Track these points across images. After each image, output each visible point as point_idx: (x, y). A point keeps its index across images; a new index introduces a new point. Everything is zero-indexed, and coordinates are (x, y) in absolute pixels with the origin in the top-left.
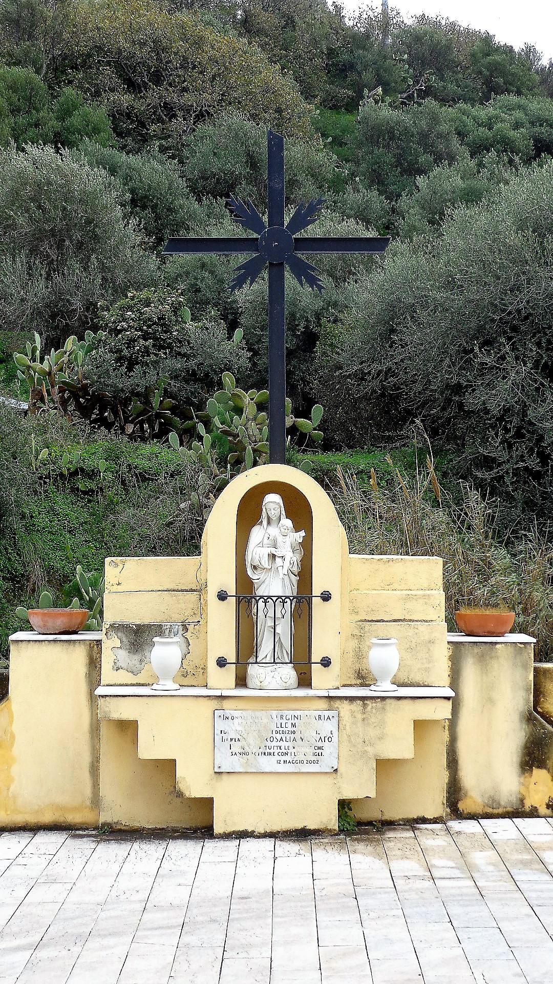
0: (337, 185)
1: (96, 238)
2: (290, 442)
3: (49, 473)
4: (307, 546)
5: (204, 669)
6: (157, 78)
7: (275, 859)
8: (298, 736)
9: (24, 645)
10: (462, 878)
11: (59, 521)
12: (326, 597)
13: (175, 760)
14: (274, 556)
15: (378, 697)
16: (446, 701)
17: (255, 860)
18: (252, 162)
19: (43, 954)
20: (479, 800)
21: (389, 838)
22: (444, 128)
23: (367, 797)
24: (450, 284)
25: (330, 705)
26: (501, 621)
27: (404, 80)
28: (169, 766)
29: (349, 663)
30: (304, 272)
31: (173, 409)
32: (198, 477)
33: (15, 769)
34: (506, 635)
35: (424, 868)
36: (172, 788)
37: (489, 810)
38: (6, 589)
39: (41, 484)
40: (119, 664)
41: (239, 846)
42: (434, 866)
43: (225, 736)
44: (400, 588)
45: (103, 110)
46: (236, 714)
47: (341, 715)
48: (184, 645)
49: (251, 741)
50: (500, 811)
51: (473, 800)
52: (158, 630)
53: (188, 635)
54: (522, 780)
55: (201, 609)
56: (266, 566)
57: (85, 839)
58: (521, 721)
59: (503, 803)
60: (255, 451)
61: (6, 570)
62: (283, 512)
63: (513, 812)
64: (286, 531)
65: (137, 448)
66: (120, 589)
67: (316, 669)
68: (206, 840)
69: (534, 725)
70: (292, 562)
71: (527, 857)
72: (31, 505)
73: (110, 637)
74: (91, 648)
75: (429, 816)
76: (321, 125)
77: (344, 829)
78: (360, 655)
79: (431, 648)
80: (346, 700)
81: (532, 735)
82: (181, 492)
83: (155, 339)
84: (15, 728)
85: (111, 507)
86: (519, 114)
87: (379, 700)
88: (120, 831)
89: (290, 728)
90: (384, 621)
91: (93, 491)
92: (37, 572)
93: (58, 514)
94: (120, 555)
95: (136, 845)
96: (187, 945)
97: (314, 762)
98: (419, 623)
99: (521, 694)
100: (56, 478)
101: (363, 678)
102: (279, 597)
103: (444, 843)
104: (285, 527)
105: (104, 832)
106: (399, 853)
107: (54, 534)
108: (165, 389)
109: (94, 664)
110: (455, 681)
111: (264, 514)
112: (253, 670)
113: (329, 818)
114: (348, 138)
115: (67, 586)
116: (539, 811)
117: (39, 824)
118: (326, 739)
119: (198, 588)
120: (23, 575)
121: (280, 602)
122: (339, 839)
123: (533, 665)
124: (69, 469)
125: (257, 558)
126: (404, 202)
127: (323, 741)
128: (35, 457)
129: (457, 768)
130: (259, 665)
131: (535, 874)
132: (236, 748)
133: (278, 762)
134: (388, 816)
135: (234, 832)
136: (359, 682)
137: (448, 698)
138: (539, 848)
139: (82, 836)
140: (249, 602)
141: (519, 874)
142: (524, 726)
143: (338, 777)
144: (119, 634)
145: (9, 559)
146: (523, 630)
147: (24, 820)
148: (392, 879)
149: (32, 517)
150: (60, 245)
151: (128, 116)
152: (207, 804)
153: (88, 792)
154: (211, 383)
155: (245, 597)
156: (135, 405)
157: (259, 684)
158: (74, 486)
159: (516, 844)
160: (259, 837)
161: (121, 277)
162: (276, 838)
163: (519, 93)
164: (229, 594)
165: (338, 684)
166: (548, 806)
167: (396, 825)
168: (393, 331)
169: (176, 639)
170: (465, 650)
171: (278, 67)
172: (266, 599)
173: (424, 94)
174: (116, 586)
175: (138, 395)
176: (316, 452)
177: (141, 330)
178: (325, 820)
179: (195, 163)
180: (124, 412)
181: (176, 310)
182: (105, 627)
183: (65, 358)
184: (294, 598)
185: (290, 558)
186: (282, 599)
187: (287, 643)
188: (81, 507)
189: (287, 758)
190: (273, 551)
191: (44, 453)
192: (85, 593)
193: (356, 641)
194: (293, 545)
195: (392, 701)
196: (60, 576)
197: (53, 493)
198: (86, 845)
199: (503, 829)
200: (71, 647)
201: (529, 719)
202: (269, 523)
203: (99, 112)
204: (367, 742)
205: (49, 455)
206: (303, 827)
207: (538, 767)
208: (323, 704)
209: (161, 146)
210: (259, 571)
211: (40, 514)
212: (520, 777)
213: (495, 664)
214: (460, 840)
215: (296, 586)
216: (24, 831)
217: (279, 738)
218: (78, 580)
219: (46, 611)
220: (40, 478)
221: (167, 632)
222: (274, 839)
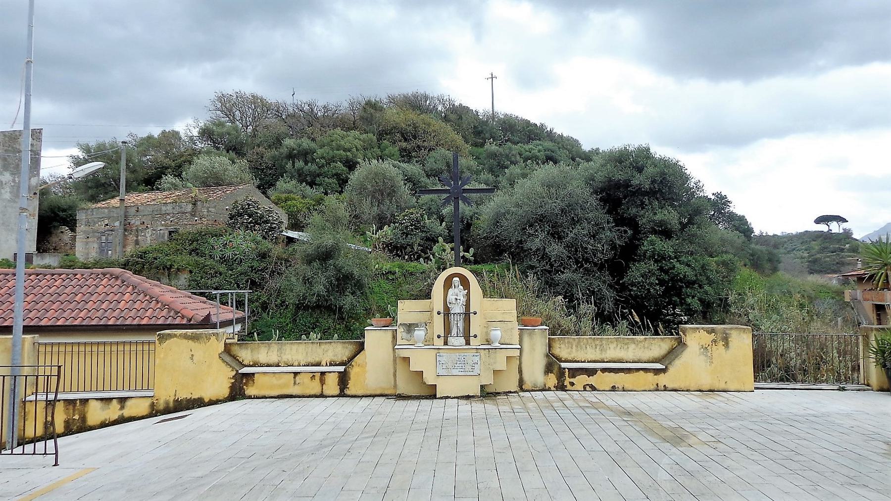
0: (478, 173)
1: (394, 191)
4: (468, 295)
5: (433, 339)
6: (415, 137)
8: (466, 363)
14: (457, 299)
18: (448, 165)
19: (376, 439)
22: (513, 152)
24: (518, 205)
27: (500, 136)
30: (466, 201)
31: (422, 250)
37: (533, 388)
45: (397, 148)
48: (426, 331)
51: (528, 385)
52: (417, 325)
54: (545, 377)
55: (432, 317)
56: (454, 303)
57: (392, 399)
60: (450, 264)
62: (460, 284)
72: (372, 284)
76: (472, 152)
78: (487, 333)
83: (415, 226)
86: (540, 147)
96: (427, 436)
99: (544, 347)
101: (488, 342)
106: (502, 404)
108: (419, 243)
109: (394, 338)
110: (521, 343)
114: (480, 157)
126: (500, 179)
134: (498, 391)
137: (518, 349)
139: (390, 398)
142: (545, 358)
145: (365, 303)
150: (382, 194)
151: (405, 150)
154: (435, 241)
156: (409, 249)
161: (403, 205)
163: (540, 140)
166: (554, 387)
168: (498, 222)
171: (456, 132)
172: (454, 314)
173: (506, 141)
175: (409, 245)
177: (410, 223)
179: (428, 166)
180: (405, 252)
181: (422, 216)
183: (384, 233)
185: (463, 300)
198: (392, 401)
199: (539, 395)
201: (547, 356)
203: (395, 150)
208: (475, 351)
209: (416, 161)
219: (378, 319)
220: (376, 275)
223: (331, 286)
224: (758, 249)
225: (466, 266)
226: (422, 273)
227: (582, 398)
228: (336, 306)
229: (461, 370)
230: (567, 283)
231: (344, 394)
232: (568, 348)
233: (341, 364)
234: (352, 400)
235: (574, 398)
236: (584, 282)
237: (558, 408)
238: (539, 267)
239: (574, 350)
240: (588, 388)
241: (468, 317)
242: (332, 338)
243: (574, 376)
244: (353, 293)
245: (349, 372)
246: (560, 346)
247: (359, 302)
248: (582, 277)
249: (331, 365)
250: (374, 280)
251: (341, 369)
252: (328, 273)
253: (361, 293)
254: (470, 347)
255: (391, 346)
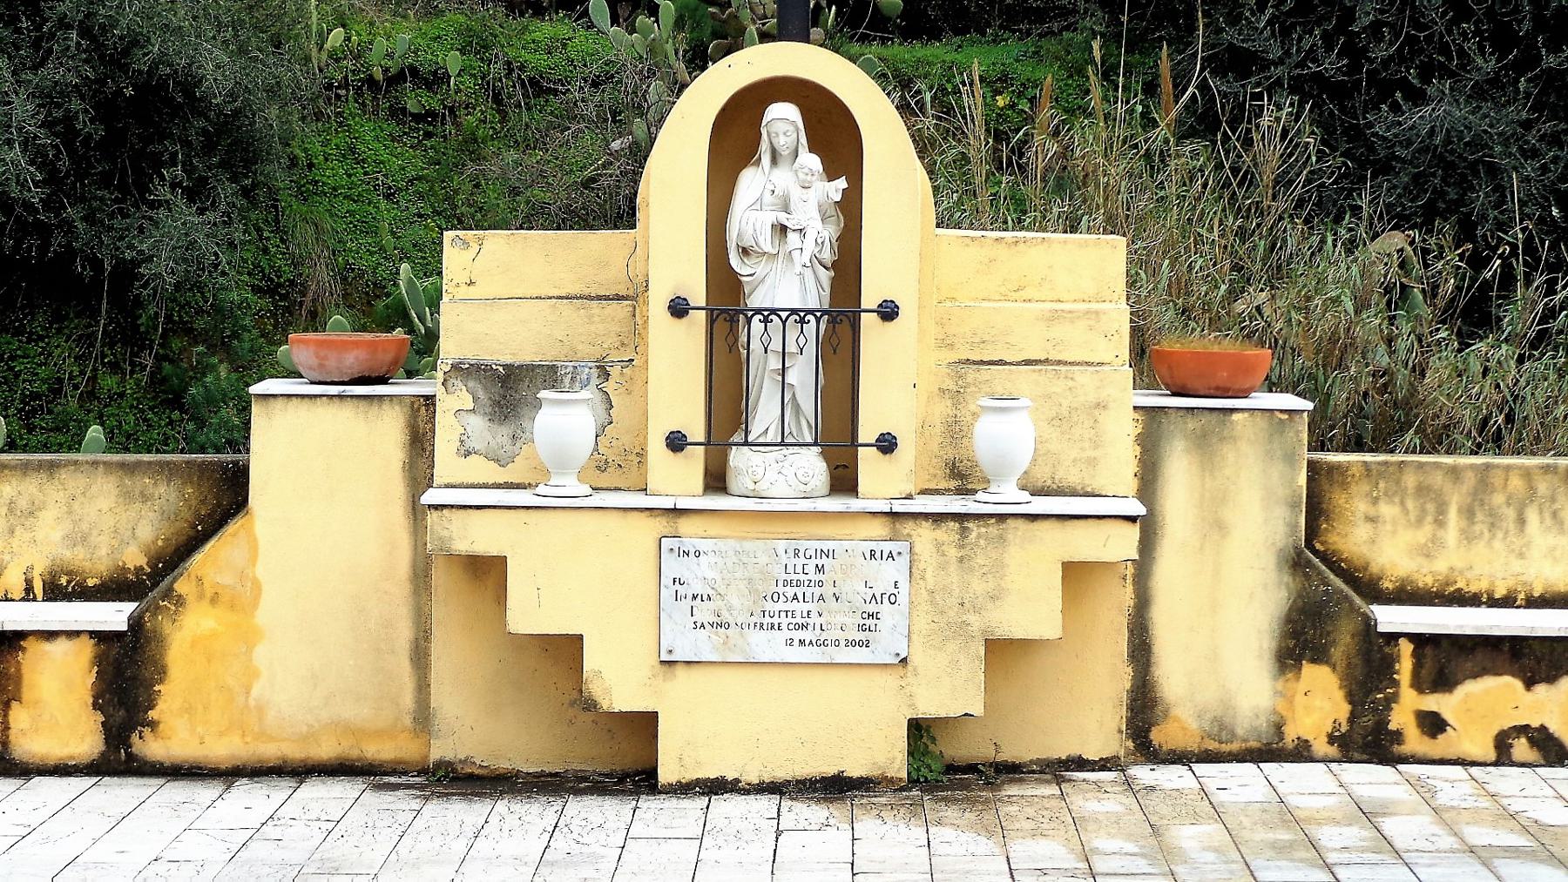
2: (836, 19)
3: (346, 78)
4: (850, 209)
5: (642, 455)
7: (779, 833)
8: (828, 591)
9: (280, 403)
10: (1155, 875)
11: (366, 174)
12: (888, 312)
13: (580, 637)
14: (783, 229)
15: (991, 516)
16: (1127, 526)
17: (739, 835)
20: (1193, 725)
21: (1009, 796)
23: (966, 714)
25: (894, 530)
26: (1242, 366)
28: (567, 650)
29: (934, 446)
32: (648, 87)
33: (261, 654)
34: (1253, 394)
35: (1076, 854)
36: (575, 694)
37: (1212, 745)
38: (260, 311)
39: (329, 99)
40: (470, 444)
41: (708, 808)
42: (1095, 851)
43: (682, 590)
44: (1037, 296)
46: (703, 545)
47: (917, 549)
48: (601, 408)
49: (735, 601)
50: (1235, 747)
52: (549, 375)
53: (610, 386)
54: (1280, 685)
55: (636, 333)
56: (767, 247)
57: (400, 793)
58: (1280, 570)
59: (1240, 732)
61: (259, 272)
62: (803, 140)
63: (1260, 749)
64: (809, 178)
65: (525, 28)
66: (472, 292)
67: (868, 458)
68: (643, 797)
69: (1307, 576)
70: (819, 241)
71: (1284, 836)
72: (311, 141)
73: (451, 389)
74: (414, 412)
75: (1091, 755)
77: (918, 779)
78: (956, 431)
79: (1100, 419)
80: (927, 521)
81: (1300, 596)
82: (614, 118)
84: (260, 571)
85: (472, 146)
87: (993, 521)
88: (471, 777)
89: (813, 576)
90: (1006, 363)
91: (432, 114)
92: (321, 276)
93: (364, 161)
94: (478, 227)
95: (502, 806)
97: (860, 644)
98: (1077, 368)
99: (1280, 515)
100: (360, 88)
101: (962, 477)
102: (794, 311)
103: (1120, 809)
104: (806, 170)
105: (439, 780)
106: (1029, 825)
107: (355, 202)
109: (420, 442)
110: (1148, 482)
111: (764, 146)
112: (739, 458)
113: (891, 757)
115: (380, 305)
116: (1313, 748)
117: (310, 763)
118: (886, 598)
119: (631, 293)
120: (292, 283)
121: (796, 320)
122: (907, 798)
123: (1306, 456)
124: (385, 71)
125: (751, 232)
127: (879, 601)
128: (318, 44)
129: (1148, 660)
130: (752, 448)
131: (1299, 870)
132: (704, 613)
133: (789, 642)
134: (1008, 755)
135: (698, 782)
136: (953, 484)
137: (1132, 519)
138: (1309, 820)
140: (733, 321)
141: (1267, 868)
142: (1287, 578)
143: (909, 674)
144: (471, 384)
145: (266, 251)
146: (1293, 388)
147: (279, 753)
148: (1011, 874)
149: (311, 166)
152: (645, 724)
153: (408, 700)
155: (723, 311)
157: (752, 486)
158: (397, 104)
159: (1264, 811)
160: (746, 792)
162: (782, 794)
164: (692, 305)
165: (910, 488)
166: (1332, 739)
167: (1023, 773)
169: (585, 394)
170: (1171, 425)
172: (768, 314)
174: (464, 288)
176: (889, 39)
178: (881, 759)
182: (443, 367)
184: (824, 312)
186: (801, 315)
187: (807, 404)
188: (411, 147)
189: (807, 635)
190: (783, 218)
191: (336, 37)
192: (416, 319)
193: (949, 403)
194: (823, 208)
195: (1020, 523)
196: (368, 286)
197: (354, 118)
198: (402, 804)
200: (375, 408)
201: (1296, 563)
202: (775, 160)
204: (967, 605)
205: (345, 40)
206: (836, 772)
207: (1313, 661)
208: (879, 528)
210: (753, 260)
211: (326, 160)
212: (1275, 678)
213: (1229, 453)
214: (1152, 802)
215: (828, 290)
216: (280, 776)
217: (790, 595)
218: (404, 292)
220: (329, 87)
221: (567, 380)
222: (778, 797)
223: (69, 144)
224: (1414, 298)
225: (856, 48)
226: (595, 84)
227: (1485, 803)
228: (97, 265)
229: (801, 635)
230: (1441, 158)
231: (130, 756)
232: (1420, 521)
233: (113, 589)
234: (177, 791)
235: (1442, 799)
236: (1534, 154)
237: (1344, 857)
238: (1281, 62)
239: (1452, 533)
240: (1521, 748)
241: (844, 328)
242: (75, 445)
243: (1442, 682)
244: (197, 192)
245: (159, 640)
246: (1372, 512)
247: (231, 245)
248: (1527, 125)
249: (54, 592)
250: (319, 116)
251: (114, 616)
252: (53, 73)
253: (246, 193)
254: (854, 504)
255: (397, 489)
